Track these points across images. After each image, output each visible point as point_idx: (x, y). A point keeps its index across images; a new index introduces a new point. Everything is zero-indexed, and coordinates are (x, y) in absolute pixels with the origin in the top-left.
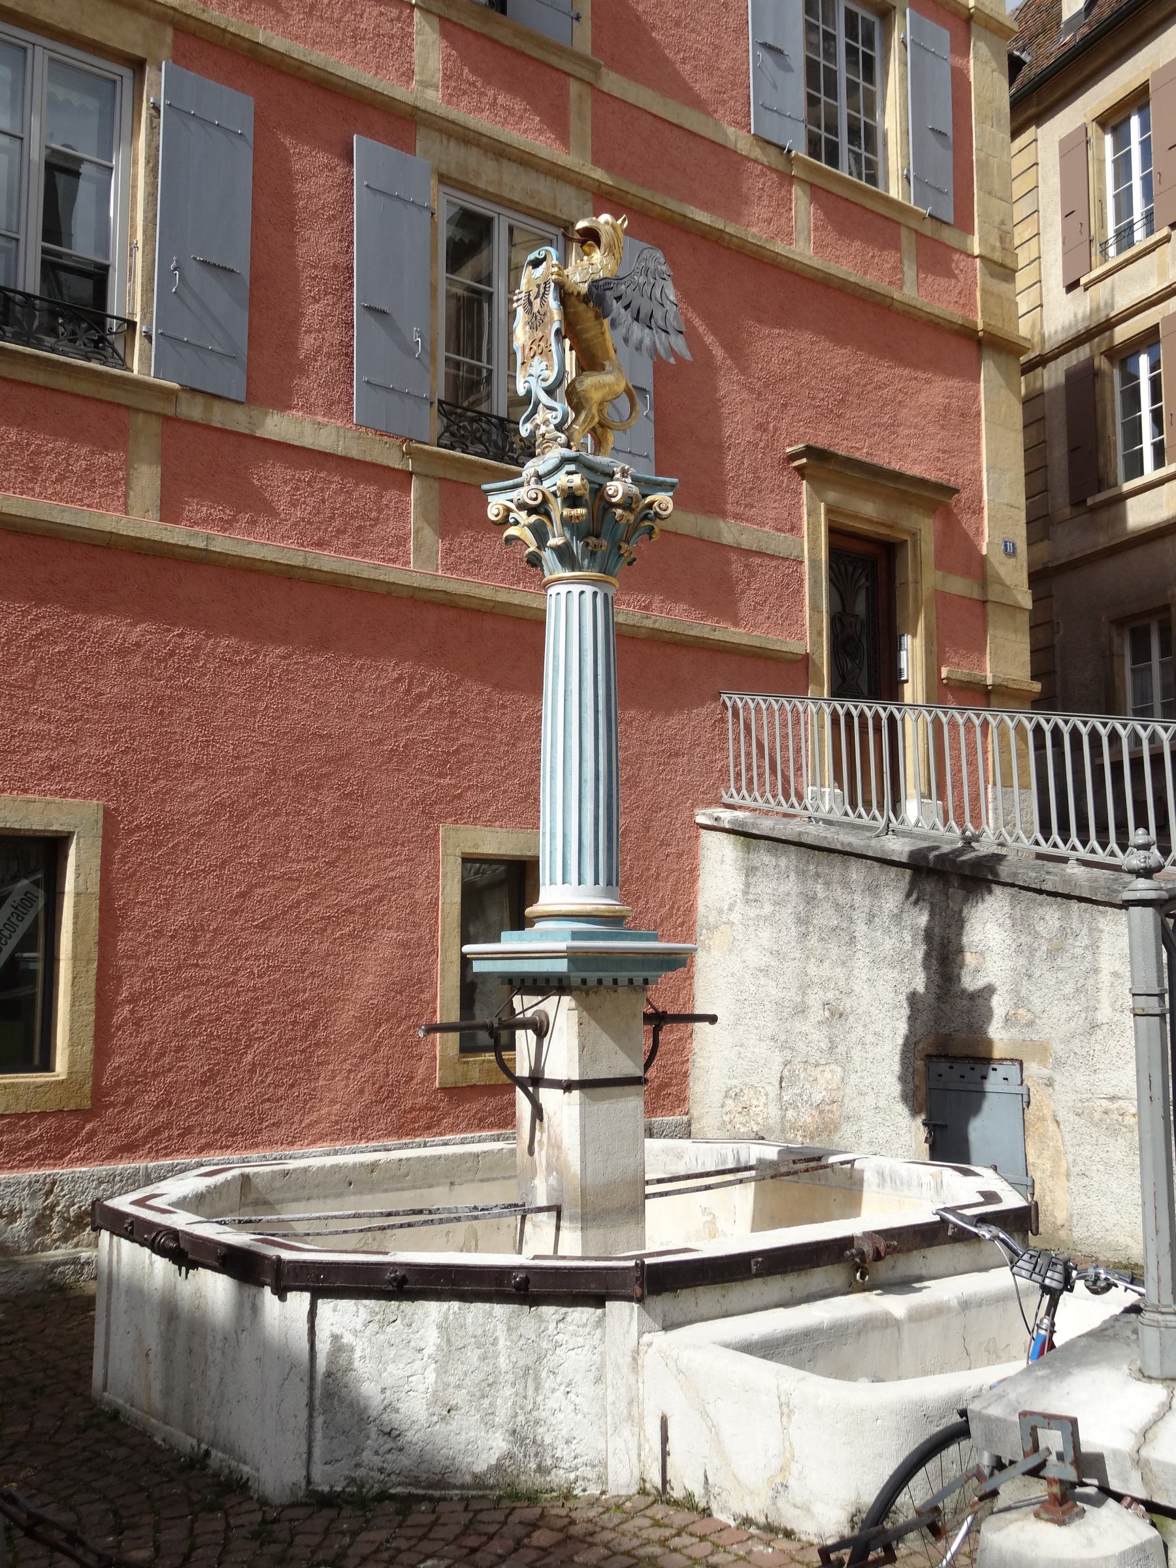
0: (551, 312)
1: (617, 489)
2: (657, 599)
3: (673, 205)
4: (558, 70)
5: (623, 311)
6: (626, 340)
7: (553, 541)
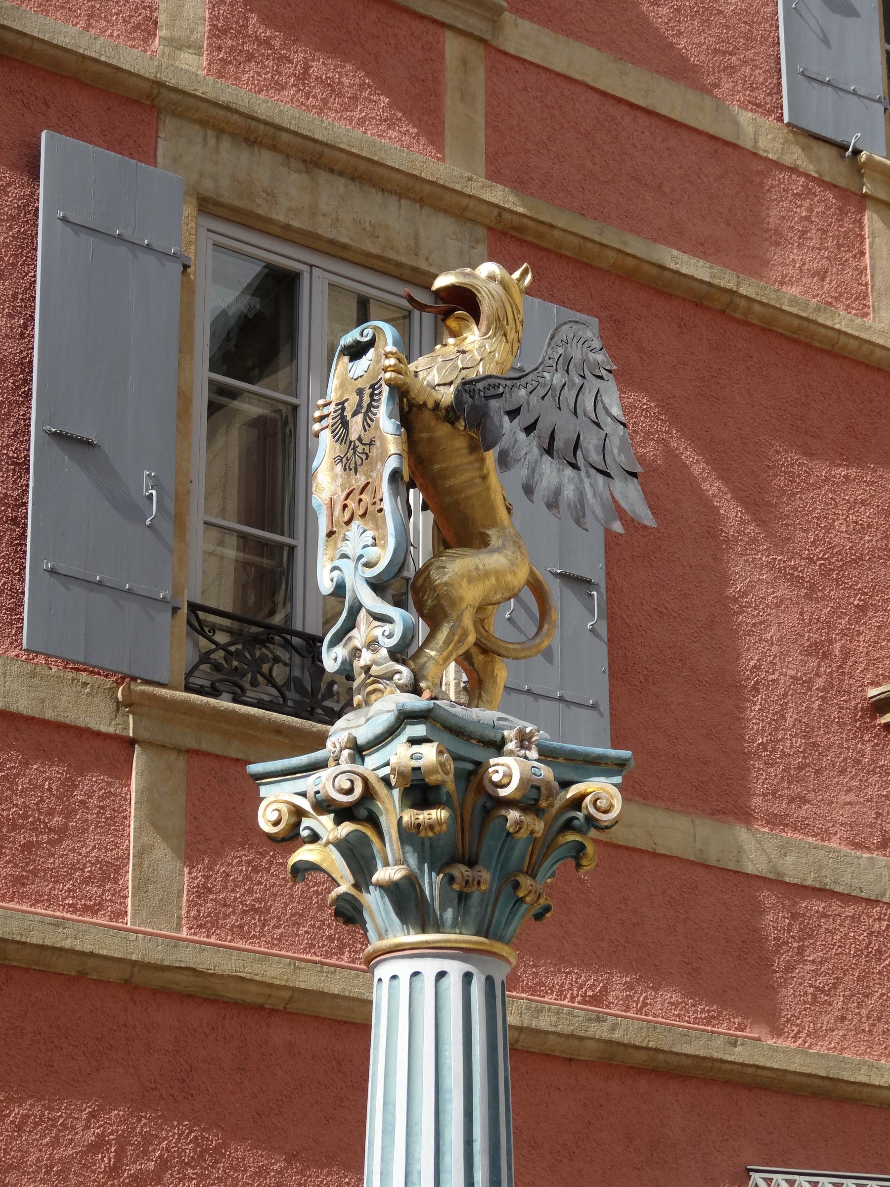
0: (383, 439)
1: (509, 771)
2: (620, 980)
3: (637, 246)
4: (423, 17)
5: (522, 436)
6: (528, 490)
7: (383, 874)
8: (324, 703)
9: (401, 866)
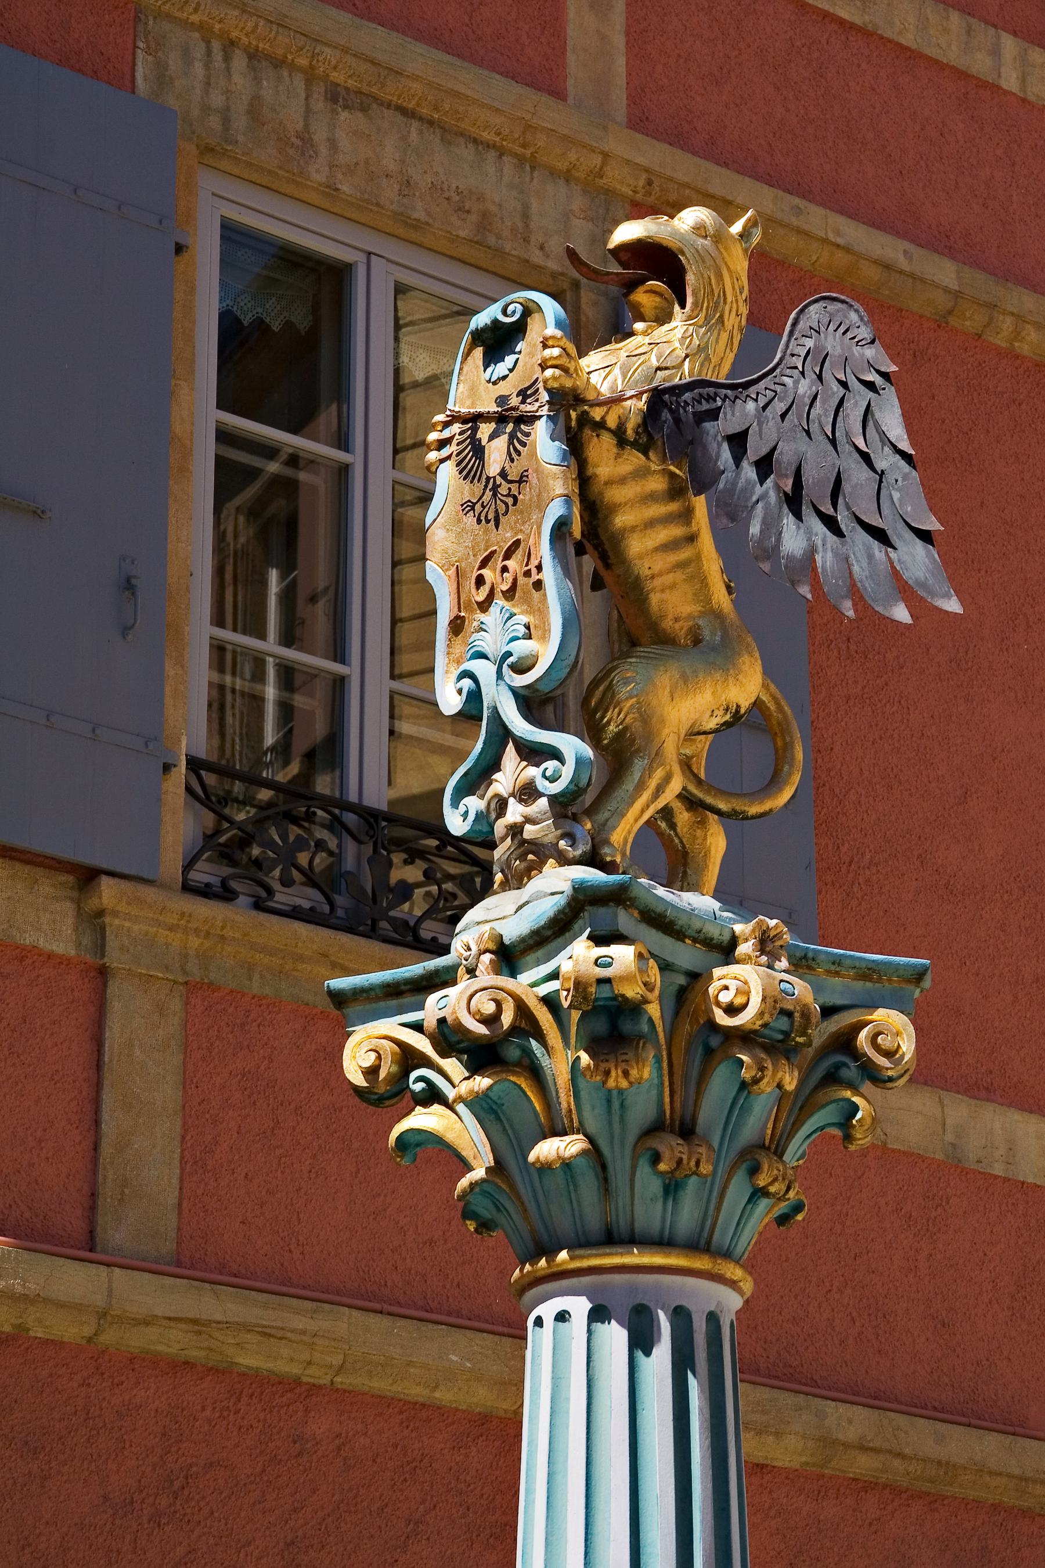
8: (392, 913)
9: (575, 1137)
